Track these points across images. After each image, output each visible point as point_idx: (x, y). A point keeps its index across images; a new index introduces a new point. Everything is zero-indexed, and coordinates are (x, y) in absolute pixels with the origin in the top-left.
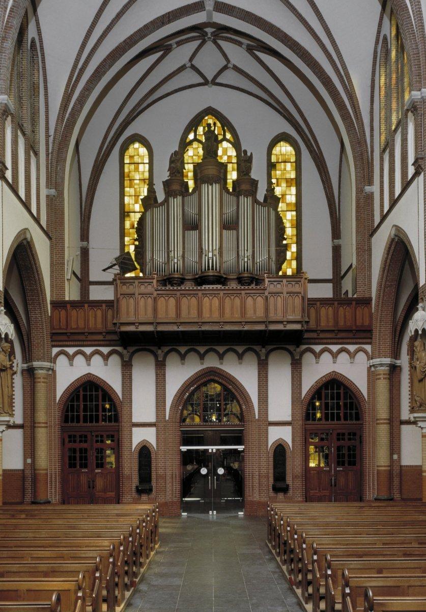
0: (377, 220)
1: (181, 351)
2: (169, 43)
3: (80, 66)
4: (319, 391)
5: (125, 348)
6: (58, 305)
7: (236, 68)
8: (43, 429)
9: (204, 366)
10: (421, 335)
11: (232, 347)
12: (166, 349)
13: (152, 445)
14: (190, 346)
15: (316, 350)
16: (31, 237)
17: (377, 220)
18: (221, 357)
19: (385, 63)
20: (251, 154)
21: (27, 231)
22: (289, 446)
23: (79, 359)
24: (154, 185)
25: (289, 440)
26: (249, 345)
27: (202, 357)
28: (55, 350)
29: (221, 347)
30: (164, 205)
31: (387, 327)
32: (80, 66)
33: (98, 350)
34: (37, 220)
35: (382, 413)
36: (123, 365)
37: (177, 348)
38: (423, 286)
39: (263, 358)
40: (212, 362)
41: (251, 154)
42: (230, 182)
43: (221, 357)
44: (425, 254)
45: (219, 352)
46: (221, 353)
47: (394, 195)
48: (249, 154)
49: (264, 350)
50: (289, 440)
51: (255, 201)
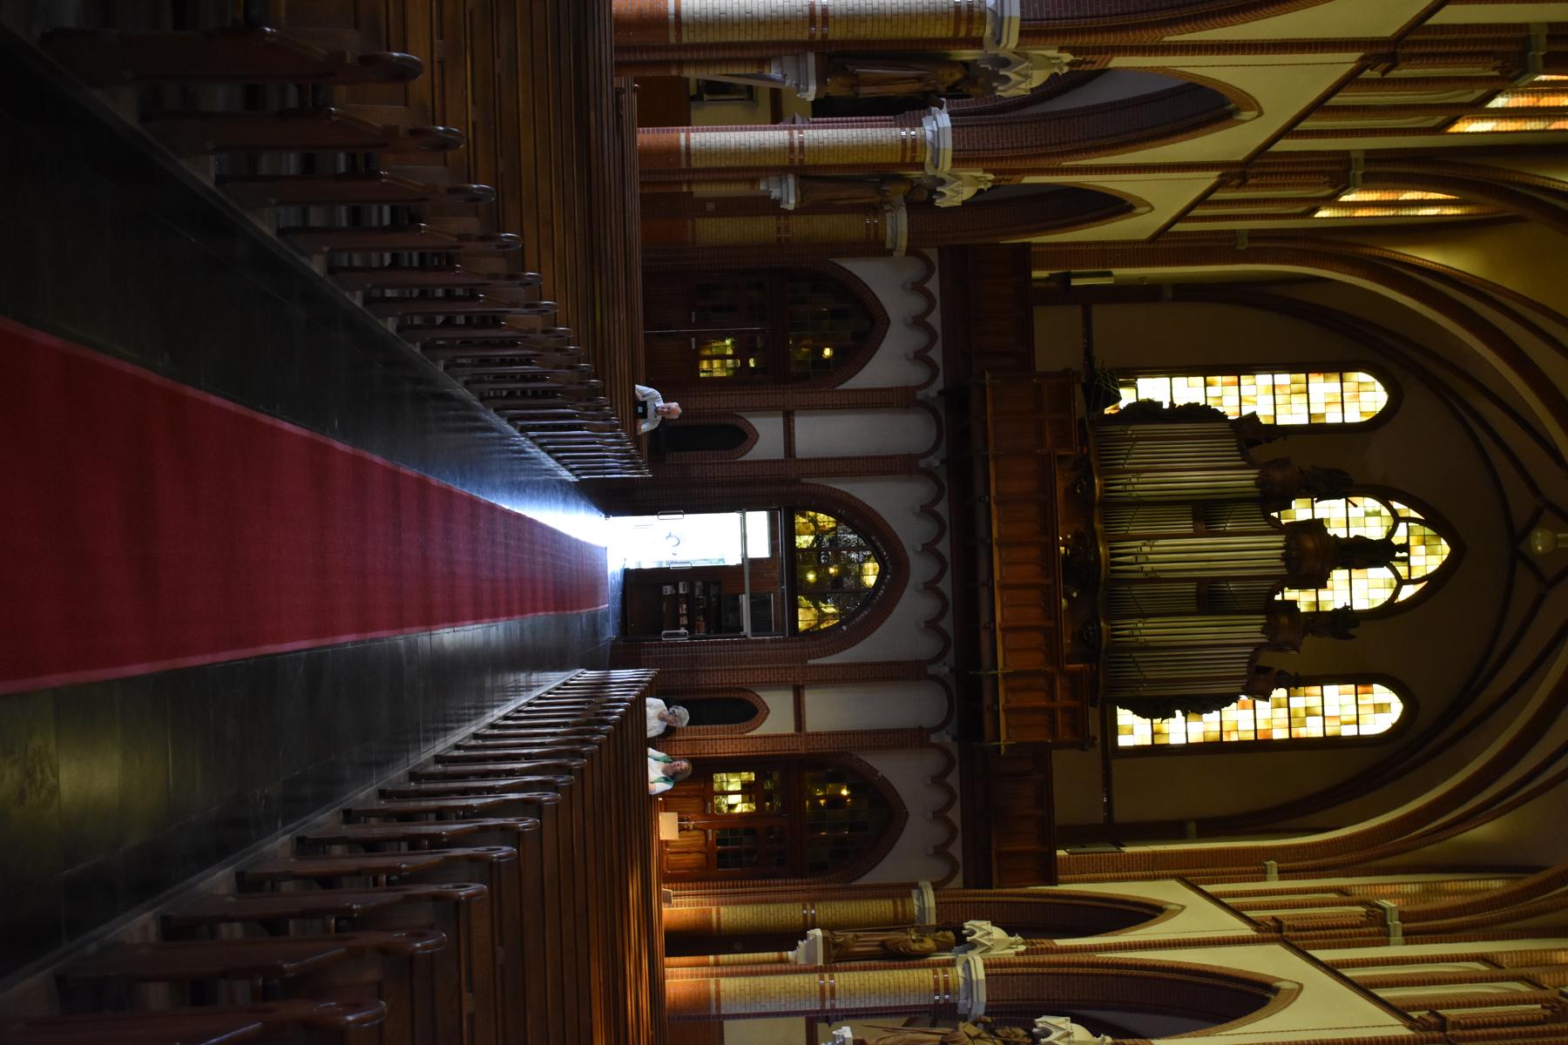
0: (1323, 955)
1: (931, 281)
2: (1268, 995)
3: (1469, 419)
4: (874, 792)
5: (940, 393)
6: (1024, 258)
7: (1539, 600)
8: (892, 907)
9: (910, 553)
10: (997, 72)
11: (941, 374)
12: (954, 748)
13: (747, 452)
14: (950, 522)
15: (932, 351)
16: (1244, 122)
17: (1323, 955)
18: (930, 587)
19: (1517, 963)
20: (1352, 637)
21: (1254, 114)
22: (754, 729)
23: (916, 304)
24: (1285, 439)
25: (765, 729)
26: (952, 563)
27: (929, 549)
28: (933, 254)
29: (939, 317)
30: (1242, 460)
31: (1026, 137)
32: (1469, 419)
33: (936, 303)
34: (1288, 131)
35: (833, 910)
36: (910, 456)
37: (946, 497)
38: (1055, 944)
39: (922, 464)
40: (919, 569)
41: (1352, 637)
42: (1290, 595)
43: (930, 587)
44: (1518, 3)
45: (938, 542)
46: (937, 547)
47: (1310, 949)
48: (1352, 631)
49: (946, 670)
50: (765, 729)
51: (1258, 647)
